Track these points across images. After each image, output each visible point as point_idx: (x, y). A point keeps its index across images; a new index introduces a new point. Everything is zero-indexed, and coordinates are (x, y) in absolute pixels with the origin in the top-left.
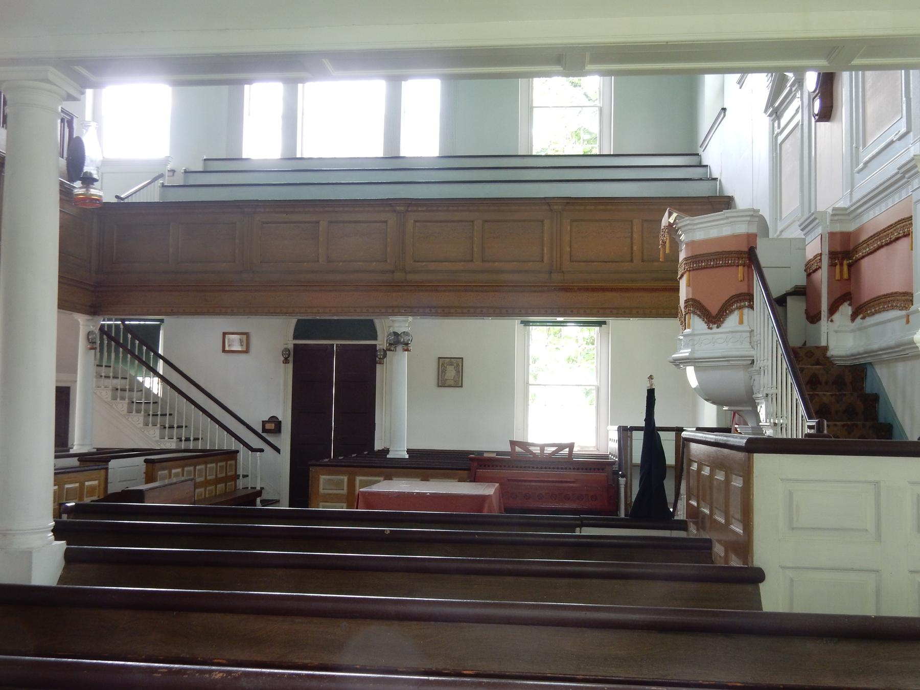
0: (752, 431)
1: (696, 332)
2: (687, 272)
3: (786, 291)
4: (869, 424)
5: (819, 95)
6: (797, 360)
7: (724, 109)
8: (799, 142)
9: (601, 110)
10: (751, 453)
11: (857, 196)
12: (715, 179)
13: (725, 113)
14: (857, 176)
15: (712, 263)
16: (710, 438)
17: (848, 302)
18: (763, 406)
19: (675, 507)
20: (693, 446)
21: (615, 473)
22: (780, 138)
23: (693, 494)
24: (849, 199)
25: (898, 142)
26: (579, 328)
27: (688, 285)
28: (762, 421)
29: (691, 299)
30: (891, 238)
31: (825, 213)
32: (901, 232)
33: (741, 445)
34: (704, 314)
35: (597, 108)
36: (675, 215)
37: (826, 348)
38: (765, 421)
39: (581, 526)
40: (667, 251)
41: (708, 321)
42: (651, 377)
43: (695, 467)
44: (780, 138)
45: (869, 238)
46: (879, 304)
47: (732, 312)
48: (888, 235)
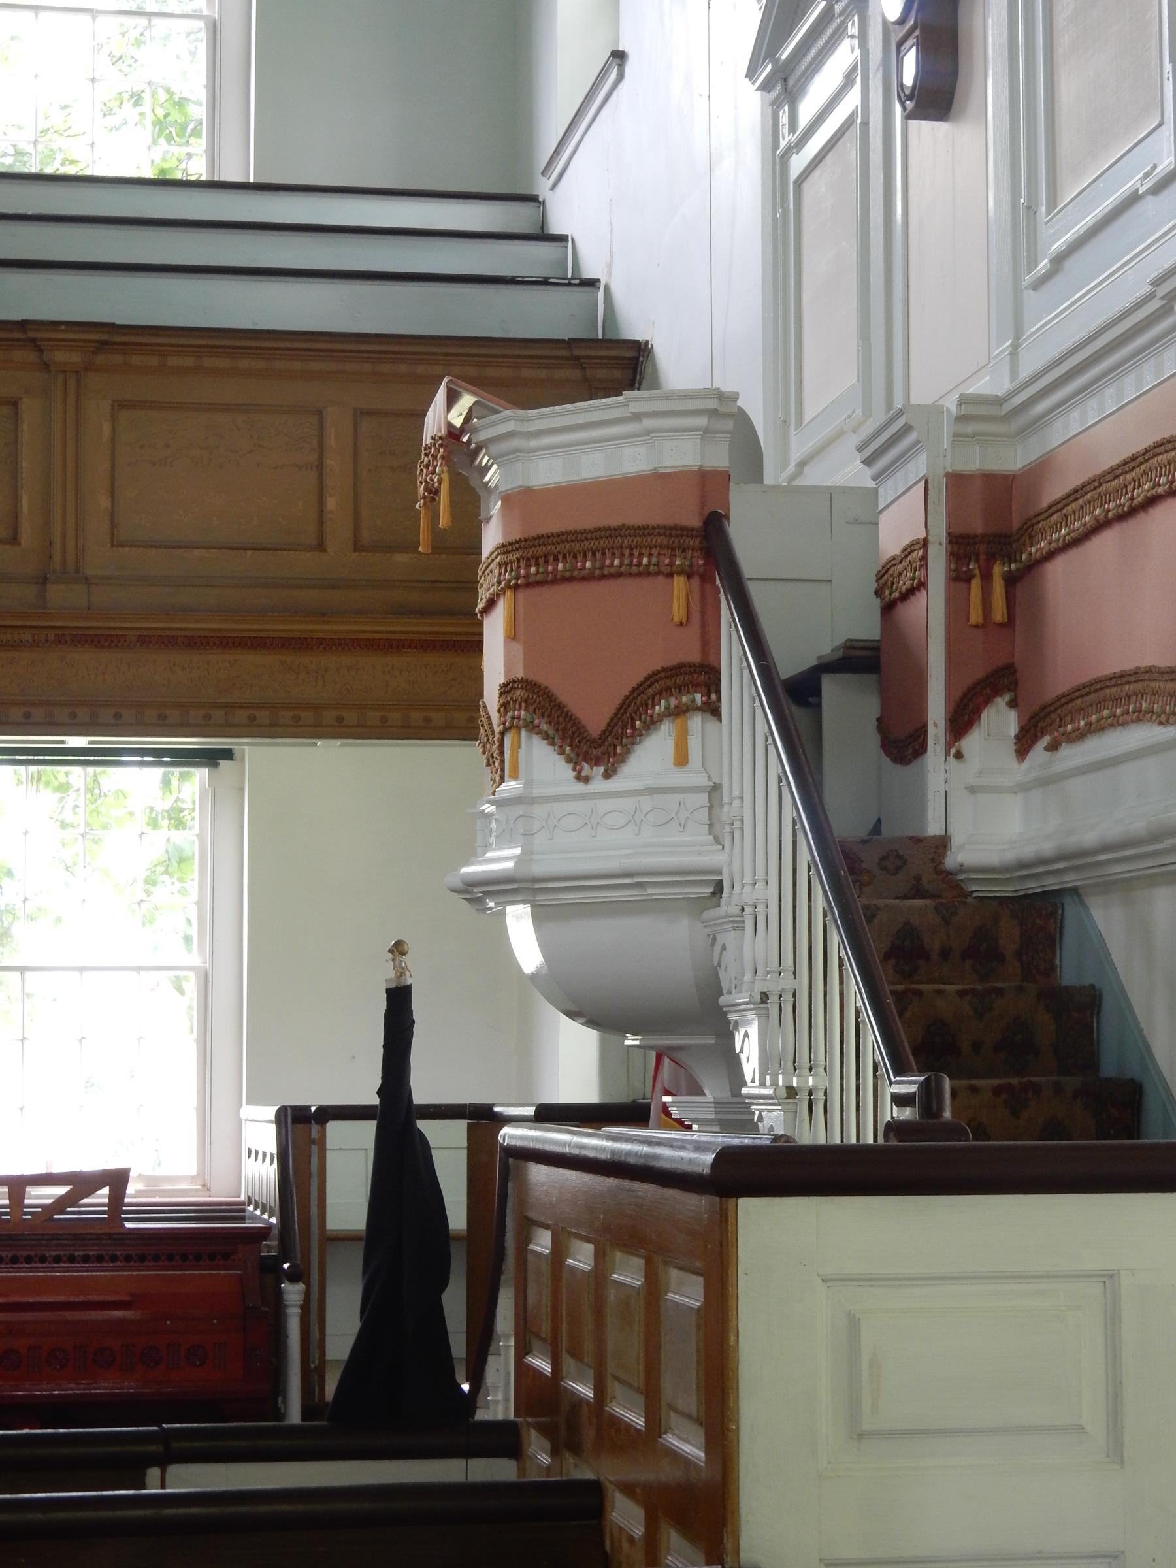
0: (716, 1113)
1: (536, 792)
2: (509, 593)
3: (819, 658)
4: (1072, 1082)
5: (917, 33)
6: (854, 882)
7: (619, 56)
8: (855, 176)
9: (214, 30)
10: (732, 1197)
11: (1030, 363)
12: (592, 283)
13: (621, 67)
14: (1030, 296)
15: (588, 564)
16: (595, 1148)
17: (1007, 697)
18: (753, 1030)
19: (477, 1378)
20: (539, 1173)
21: (271, 1267)
22: (798, 163)
23: (538, 1336)
24: (1006, 369)
25: (1150, 198)
26: (156, 774)
27: (512, 635)
28: (750, 1084)
29: (522, 681)
30: (1132, 499)
31: (935, 410)
32: (1163, 480)
33: (698, 1170)
34: (564, 731)
35: (201, 24)
36: (467, 401)
37: (942, 844)
38: (757, 1083)
39: (164, 1461)
40: (444, 521)
41: (578, 755)
42: (398, 949)
43: (542, 1243)
44: (798, 163)
45: (1068, 496)
46: (1099, 705)
47: (651, 724)
48: (1126, 487)
